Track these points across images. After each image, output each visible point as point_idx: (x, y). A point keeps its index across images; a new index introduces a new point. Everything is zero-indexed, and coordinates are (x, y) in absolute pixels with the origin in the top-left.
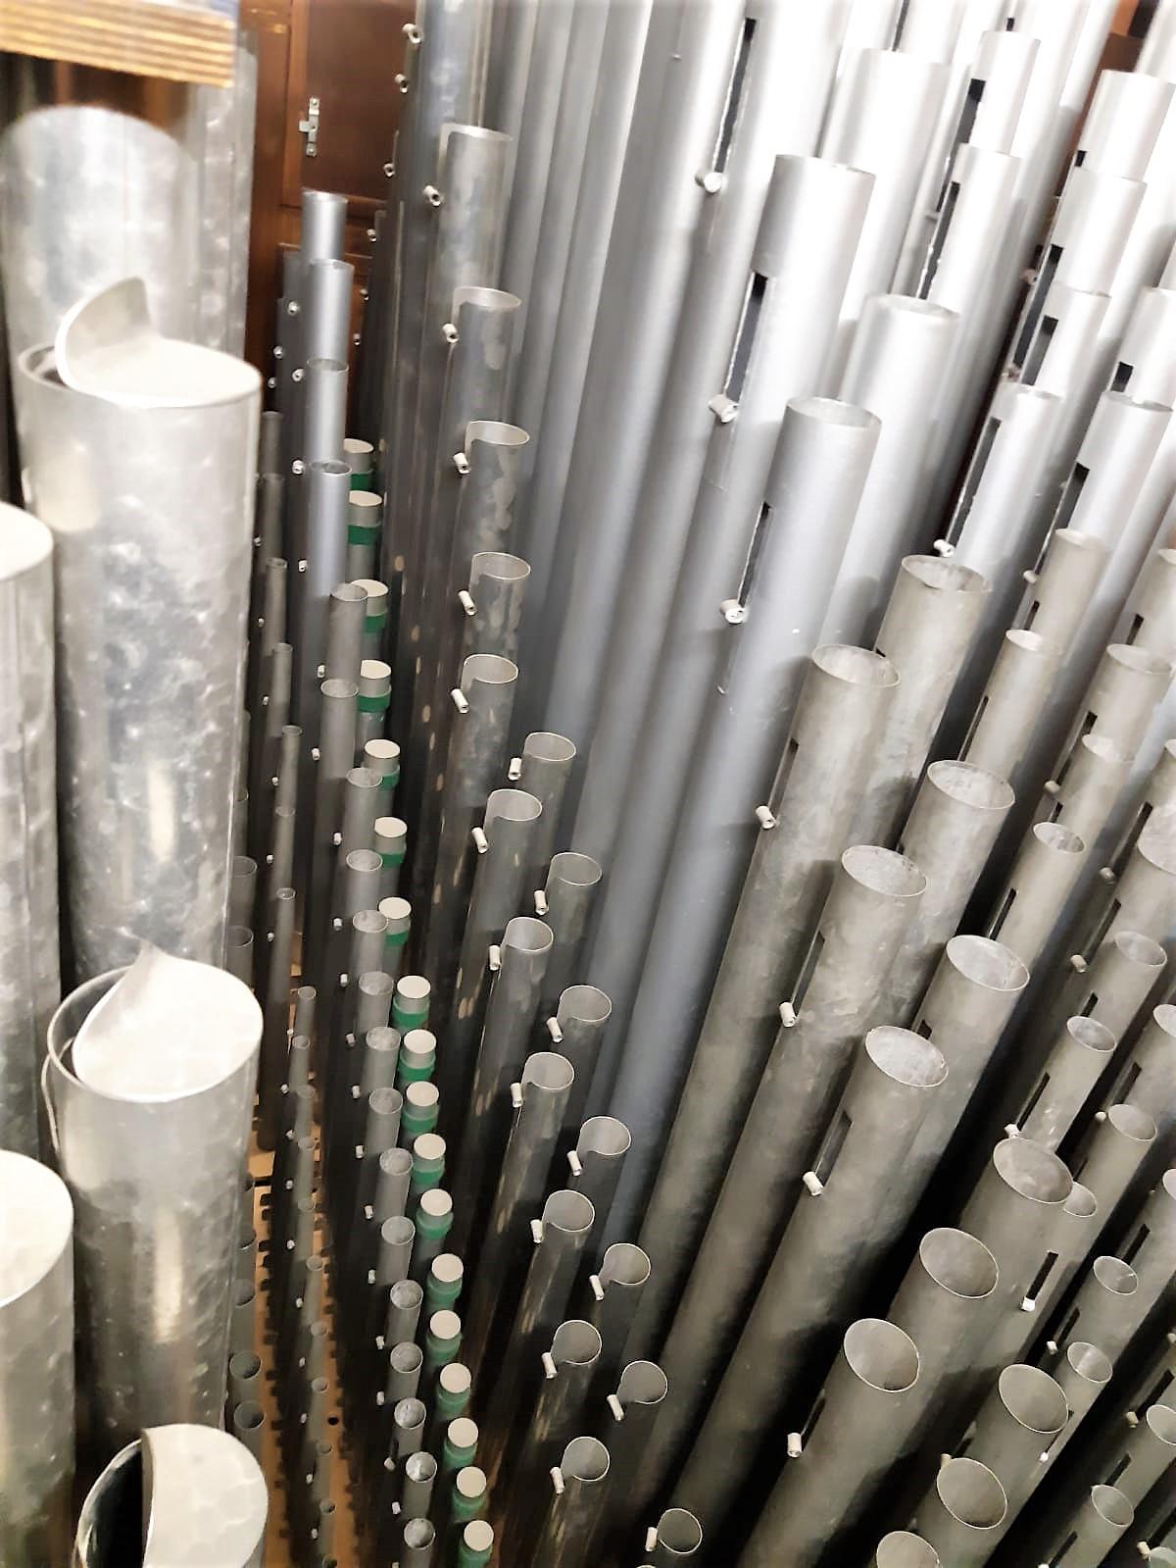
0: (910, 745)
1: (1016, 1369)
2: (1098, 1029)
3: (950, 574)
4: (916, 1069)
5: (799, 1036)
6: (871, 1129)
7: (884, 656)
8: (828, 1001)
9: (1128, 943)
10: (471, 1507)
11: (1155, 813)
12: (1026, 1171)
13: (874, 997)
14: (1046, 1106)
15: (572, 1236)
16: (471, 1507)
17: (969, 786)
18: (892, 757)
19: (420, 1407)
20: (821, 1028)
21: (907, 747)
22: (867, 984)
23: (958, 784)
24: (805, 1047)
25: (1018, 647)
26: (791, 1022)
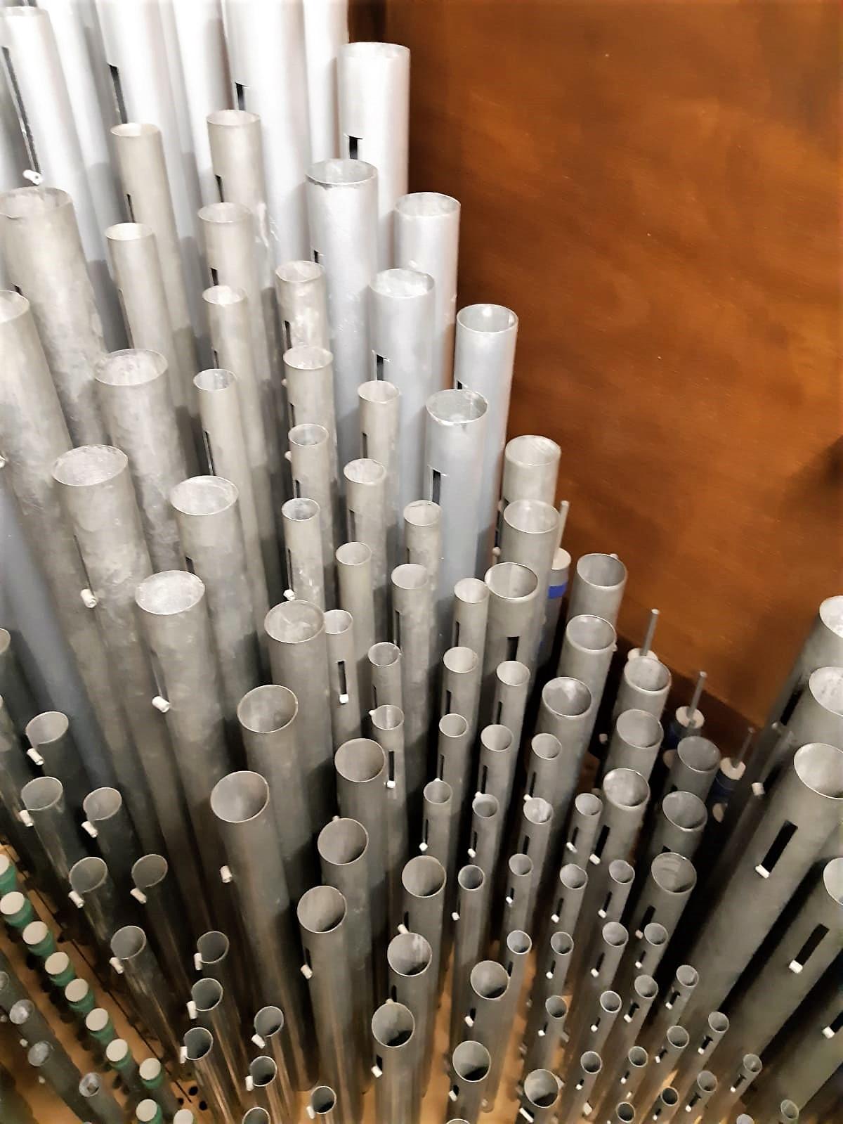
0: (84, 352)
1: (347, 747)
2: (307, 503)
3: (42, 198)
4: (190, 593)
5: (104, 609)
6: (171, 652)
7: (326, 186)
8: (105, 577)
9: (303, 432)
10: (84, 1005)
11: (292, 325)
12: (300, 619)
13: (139, 558)
14: (298, 570)
15: (53, 809)
16: (84, 1005)
17: (139, 367)
18: (75, 367)
19: (4, 975)
20: (114, 597)
21: (81, 354)
22: (125, 552)
23: (129, 368)
24: (112, 614)
25: (119, 241)
26: (93, 603)
